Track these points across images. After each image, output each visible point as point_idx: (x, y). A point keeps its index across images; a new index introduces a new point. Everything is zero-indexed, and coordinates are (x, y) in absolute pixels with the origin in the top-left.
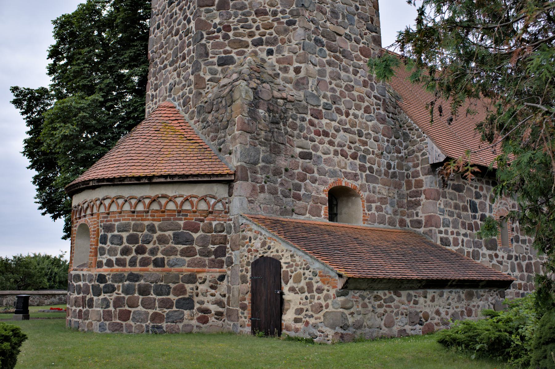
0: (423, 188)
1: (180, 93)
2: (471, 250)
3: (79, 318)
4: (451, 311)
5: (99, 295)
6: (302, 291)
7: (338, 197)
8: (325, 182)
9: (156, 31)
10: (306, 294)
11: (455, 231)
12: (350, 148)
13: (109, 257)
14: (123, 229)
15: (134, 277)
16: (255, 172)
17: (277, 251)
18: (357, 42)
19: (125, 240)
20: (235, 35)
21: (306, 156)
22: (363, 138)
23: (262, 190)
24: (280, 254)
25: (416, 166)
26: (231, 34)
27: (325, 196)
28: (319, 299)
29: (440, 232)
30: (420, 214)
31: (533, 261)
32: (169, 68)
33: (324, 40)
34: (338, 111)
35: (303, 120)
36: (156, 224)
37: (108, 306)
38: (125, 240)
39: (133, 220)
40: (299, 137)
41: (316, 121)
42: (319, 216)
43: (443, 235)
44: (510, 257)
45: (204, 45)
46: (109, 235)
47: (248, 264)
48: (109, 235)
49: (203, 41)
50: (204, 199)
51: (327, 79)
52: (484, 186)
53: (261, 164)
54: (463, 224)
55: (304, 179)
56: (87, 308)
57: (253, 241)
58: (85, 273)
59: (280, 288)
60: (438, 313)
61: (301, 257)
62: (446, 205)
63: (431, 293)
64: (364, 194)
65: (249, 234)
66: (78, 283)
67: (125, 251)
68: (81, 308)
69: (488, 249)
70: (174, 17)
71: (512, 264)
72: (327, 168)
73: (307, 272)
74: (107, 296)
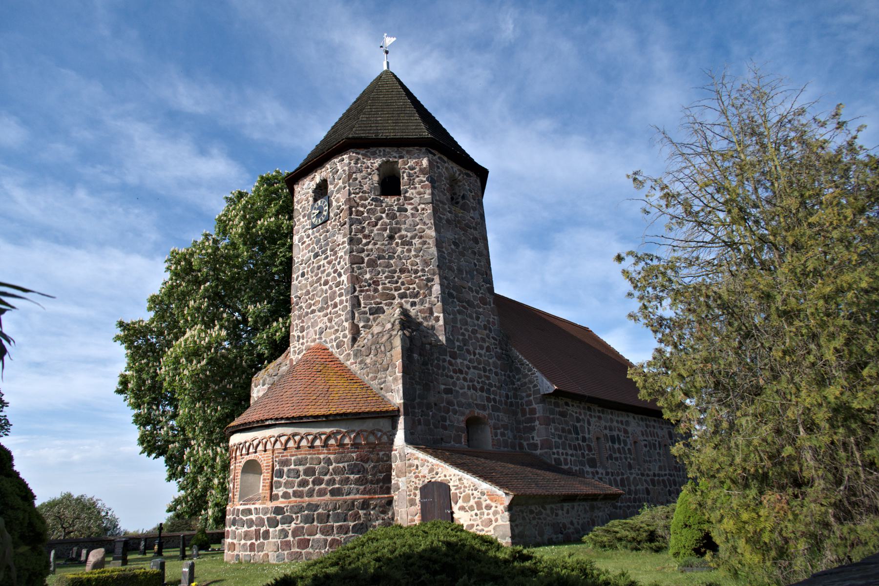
0: (537, 415)
1: (333, 337)
2: (577, 468)
3: (250, 551)
4: (581, 522)
5: (277, 526)
6: (471, 508)
7: (473, 423)
8: (463, 414)
9: (300, 278)
10: (476, 511)
11: (564, 452)
12: (478, 382)
13: (285, 490)
14: (300, 462)
15: (314, 507)
16: (414, 408)
17: (445, 476)
18: (477, 292)
19: (301, 473)
20: (384, 289)
21: (448, 391)
22: (487, 374)
23: (420, 423)
24: (448, 478)
25: (529, 395)
26: (380, 288)
27: (463, 425)
28: (488, 514)
29: (554, 453)
30: (536, 438)
31: (625, 477)
32: (318, 313)
33: (454, 293)
34: (468, 351)
35: (444, 360)
36: (332, 457)
37: (286, 536)
38: (301, 473)
39: (310, 454)
40: (442, 375)
41: (453, 361)
42: (461, 443)
43: (556, 456)
44: (607, 474)
45: (358, 297)
46: (286, 469)
47: (416, 488)
48: (286, 469)
49: (356, 294)
50: (372, 433)
51: (459, 325)
52: (582, 411)
53: (418, 400)
54: (570, 446)
55: (448, 411)
56: (262, 540)
57: (420, 468)
58: (257, 506)
59: (451, 508)
60: (572, 523)
61: (469, 479)
62: (556, 429)
63: (566, 505)
64: (492, 422)
65: (416, 462)
66: (248, 517)
67: (304, 483)
68: (254, 541)
69: (590, 467)
70: (322, 269)
71: (610, 479)
72: (463, 401)
73: (475, 493)
74: (285, 526)
